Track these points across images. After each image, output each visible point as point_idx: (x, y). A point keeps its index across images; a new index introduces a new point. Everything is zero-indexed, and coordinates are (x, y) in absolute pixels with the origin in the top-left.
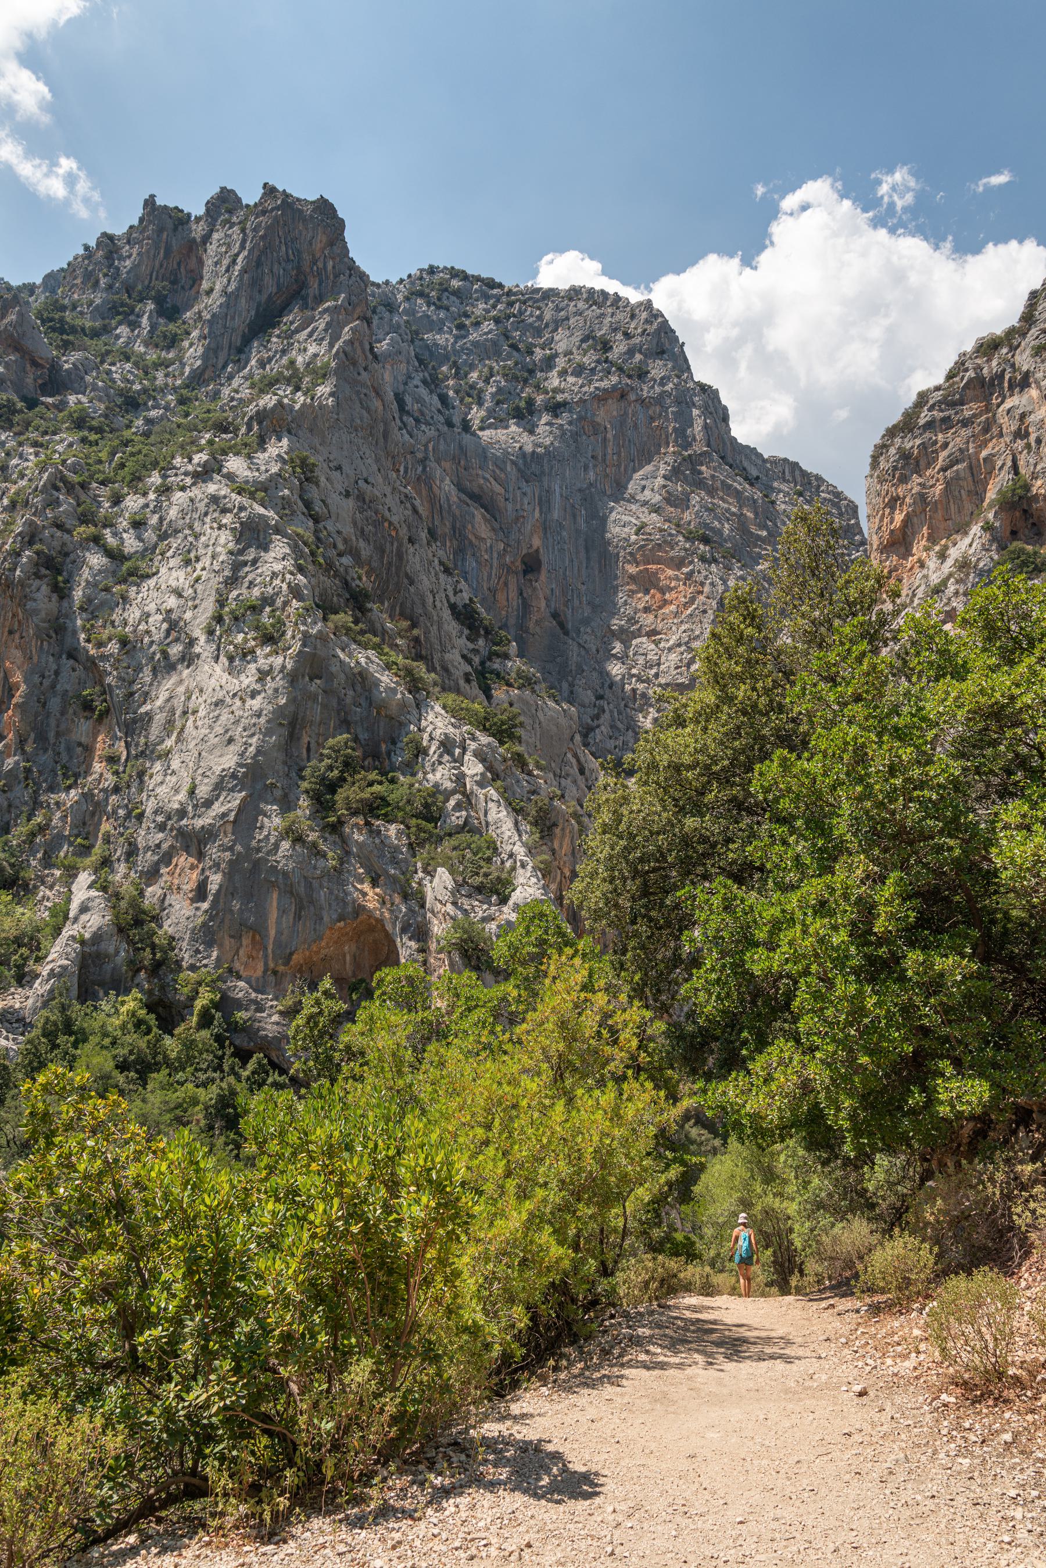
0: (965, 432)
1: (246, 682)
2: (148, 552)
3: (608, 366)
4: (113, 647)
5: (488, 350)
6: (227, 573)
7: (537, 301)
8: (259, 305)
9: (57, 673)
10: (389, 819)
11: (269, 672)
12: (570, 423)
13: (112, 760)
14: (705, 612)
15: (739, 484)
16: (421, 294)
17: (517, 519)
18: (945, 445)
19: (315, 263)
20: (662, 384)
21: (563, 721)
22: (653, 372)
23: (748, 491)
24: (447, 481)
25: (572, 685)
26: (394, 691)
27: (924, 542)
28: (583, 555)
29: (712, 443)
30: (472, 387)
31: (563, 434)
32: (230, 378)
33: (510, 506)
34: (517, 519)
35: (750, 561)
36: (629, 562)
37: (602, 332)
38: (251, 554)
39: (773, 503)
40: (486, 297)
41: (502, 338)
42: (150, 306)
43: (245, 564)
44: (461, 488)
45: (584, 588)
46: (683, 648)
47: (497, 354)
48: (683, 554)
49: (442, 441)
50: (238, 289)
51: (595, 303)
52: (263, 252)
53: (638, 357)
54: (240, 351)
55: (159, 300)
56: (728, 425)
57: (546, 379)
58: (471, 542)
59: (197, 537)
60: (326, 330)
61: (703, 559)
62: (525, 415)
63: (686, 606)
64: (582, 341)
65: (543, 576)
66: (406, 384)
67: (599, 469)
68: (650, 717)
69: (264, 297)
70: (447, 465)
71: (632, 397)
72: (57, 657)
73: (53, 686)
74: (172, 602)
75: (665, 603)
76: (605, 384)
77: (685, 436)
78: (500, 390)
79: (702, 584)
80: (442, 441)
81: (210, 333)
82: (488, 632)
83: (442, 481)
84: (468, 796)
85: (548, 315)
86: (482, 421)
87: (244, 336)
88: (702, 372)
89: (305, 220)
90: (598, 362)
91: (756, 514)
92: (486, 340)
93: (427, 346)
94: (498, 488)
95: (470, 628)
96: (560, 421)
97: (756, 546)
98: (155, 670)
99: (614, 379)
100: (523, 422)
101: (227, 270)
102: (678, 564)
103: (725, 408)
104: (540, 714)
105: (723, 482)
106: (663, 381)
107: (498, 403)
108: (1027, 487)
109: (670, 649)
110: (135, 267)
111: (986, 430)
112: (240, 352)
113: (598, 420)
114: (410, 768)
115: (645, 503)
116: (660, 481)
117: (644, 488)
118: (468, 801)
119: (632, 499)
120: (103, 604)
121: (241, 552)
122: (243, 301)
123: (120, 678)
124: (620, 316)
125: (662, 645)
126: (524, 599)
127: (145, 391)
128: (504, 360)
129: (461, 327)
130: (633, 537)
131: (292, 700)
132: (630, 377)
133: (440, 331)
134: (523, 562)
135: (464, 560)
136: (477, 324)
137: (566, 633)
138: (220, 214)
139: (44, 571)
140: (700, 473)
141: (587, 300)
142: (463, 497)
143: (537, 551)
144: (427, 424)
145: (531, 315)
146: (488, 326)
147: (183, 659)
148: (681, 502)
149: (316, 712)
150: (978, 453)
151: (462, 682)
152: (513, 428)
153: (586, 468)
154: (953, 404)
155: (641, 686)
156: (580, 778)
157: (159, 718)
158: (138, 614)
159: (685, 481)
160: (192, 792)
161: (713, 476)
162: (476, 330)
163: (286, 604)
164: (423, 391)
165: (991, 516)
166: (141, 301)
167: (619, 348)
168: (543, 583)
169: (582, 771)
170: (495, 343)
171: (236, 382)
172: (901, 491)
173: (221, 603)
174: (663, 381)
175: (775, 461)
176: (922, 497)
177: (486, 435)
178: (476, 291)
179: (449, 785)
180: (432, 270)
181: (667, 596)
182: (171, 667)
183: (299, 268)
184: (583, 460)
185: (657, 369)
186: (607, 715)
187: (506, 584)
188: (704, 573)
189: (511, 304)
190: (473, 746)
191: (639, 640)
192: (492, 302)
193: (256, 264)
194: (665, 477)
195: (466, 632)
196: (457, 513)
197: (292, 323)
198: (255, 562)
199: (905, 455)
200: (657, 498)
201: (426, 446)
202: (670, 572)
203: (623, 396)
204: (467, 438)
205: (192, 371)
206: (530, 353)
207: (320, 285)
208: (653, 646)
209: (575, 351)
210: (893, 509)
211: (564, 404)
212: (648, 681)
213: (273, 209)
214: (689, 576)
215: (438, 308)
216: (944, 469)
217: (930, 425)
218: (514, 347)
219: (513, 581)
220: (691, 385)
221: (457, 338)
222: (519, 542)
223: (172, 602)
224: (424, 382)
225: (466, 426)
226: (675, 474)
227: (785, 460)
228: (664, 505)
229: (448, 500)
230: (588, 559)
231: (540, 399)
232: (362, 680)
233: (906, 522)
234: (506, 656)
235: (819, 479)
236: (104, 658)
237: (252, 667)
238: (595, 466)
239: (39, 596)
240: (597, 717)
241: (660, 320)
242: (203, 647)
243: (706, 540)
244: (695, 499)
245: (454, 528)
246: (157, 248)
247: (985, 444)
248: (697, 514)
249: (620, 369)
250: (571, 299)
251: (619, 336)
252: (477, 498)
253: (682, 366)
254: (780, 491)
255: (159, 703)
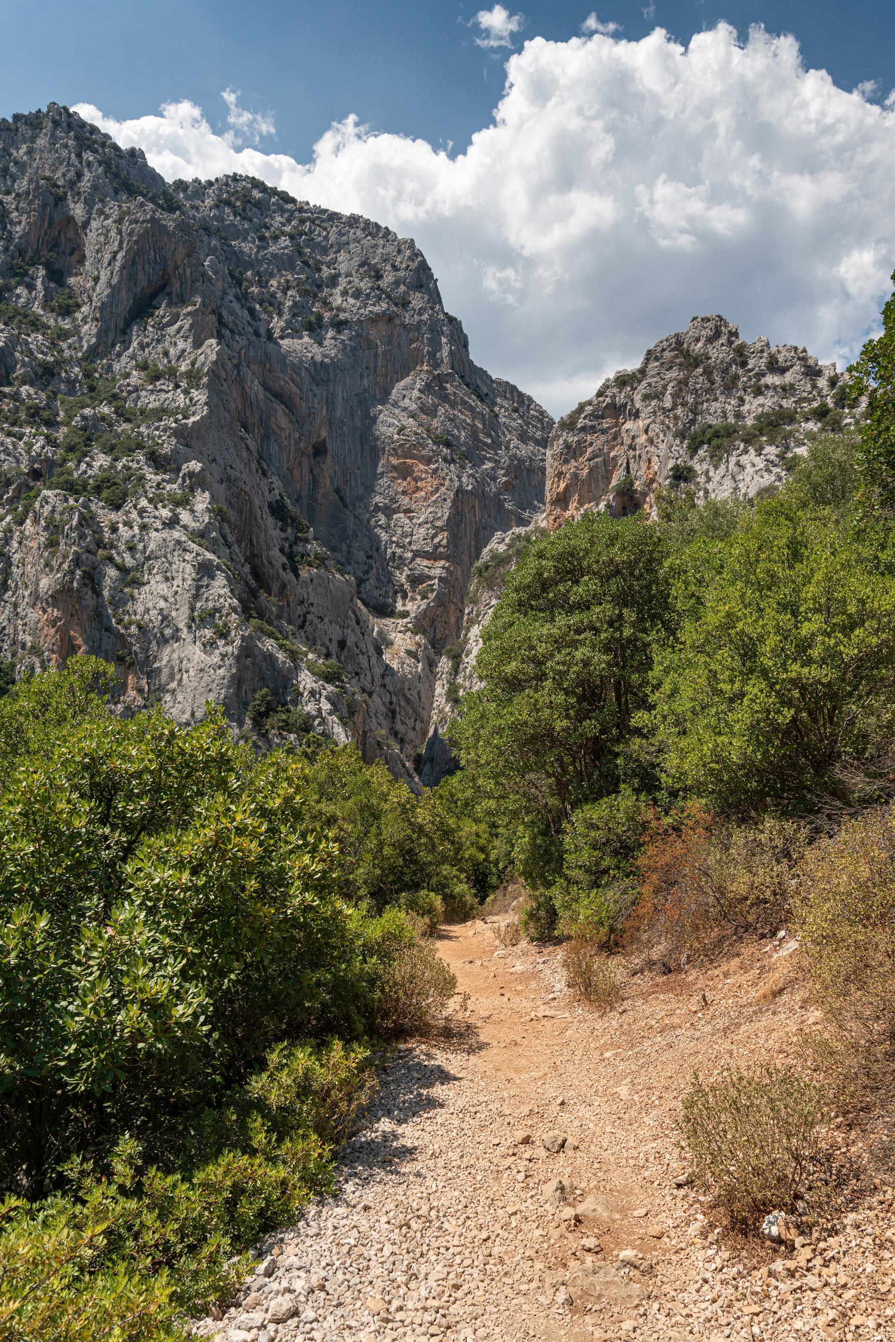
0: (603, 438)
1: (215, 660)
2: (139, 567)
3: (380, 293)
4: (133, 629)
5: (284, 263)
6: (193, 592)
7: (324, 221)
8: (135, 296)
9: (101, 639)
10: (290, 732)
11: (226, 655)
12: (350, 339)
13: (140, 691)
14: (445, 500)
15: (473, 401)
16: (228, 203)
17: (309, 414)
18: (591, 444)
19: (177, 268)
20: (420, 314)
21: (346, 588)
22: (414, 302)
23: (480, 407)
24: (256, 382)
25: (349, 546)
26: (284, 662)
27: (575, 504)
28: (358, 446)
29: (456, 365)
30: (273, 296)
31: (345, 348)
32: (119, 355)
33: (304, 404)
34: (309, 414)
35: (478, 462)
36: (392, 455)
37: (376, 261)
38: (205, 581)
39: (497, 416)
40: (282, 211)
41: (296, 254)
42: (42, 272)
43: (202, 586)
44: (266, 388)
45: (359, 472)
46: (429, 525)
47: (292, 267)
48: (431, 454)
49: (251, 349)
50: (119, 282)
51: (370, 234)
52: (137, 254)
53: (402, 288)
54: (124, 332)
55: (48, 266)
56: (467, 350)
57: (331, 295)
58: (274, 431)
59: (171, 564)
60: (190, 330)
61: (445, 460)
62: (315, 328)
63: (432, 493)
64: (360, 266)
65: (329, 459)
66: (222, 299)
67: (372, 377)
68: (405, 574)
69: (139, 290)
70: (255, 367)
71: (397, 322)
72: (99, 630)
73: (99, 647)
74: (162, 604)
75: (418, 489)
76: (376, 309)
77: (435, 359)
78: (295, 303)
79: (444, 479)
80: (251, 349)
81: (101, 317)
82: (293, 521)
83: (252, 382)
84: (323, 719)
85: (332, 238)
86: (282, 331)
87: (125, 320)
88: (450, 306)
89: (168, 234)
90: (372, 288)
91: (484, 425)
92: (283, 254)
93: (234, 252)
94: (295, 389)
95: (281, 520)
96: (342, 337)
97: (483, 450)
98: (158, 643)
99: (384, 305)
100: (314, 335)
101: (109, 264)
102: (428, 461)
103: (466, 337)
104: (331, 585)
105: (462, 399)
106: (421, 311)
107: (294, 315)
108: (632, 484)
109: (420, 525)
110: (26, 235)
111: (615, 438)
112: (124, 333)
113: (372, 338)
114: (295, 702)
115: (405, 409)
116: (416, 393)
117: (404, 396)
118: (323, 722)
119: (395, 404)
120: (120, 599)
121: (199, 580)
122: (124, 292)
123: (141, 648)
124: (389, 249)
125: (414, 521)
126: (314, 476)
127: (57, 362)
128: (298, 274)
129: (262, 238)
130: (396, 436)
131: (238, 670)
132: (396, 305)
133: (245, 239)
134: (314, 447)
135: (269, 444)
136: (276, 238)
137: (345, 506)
138: (94, 203)
139: (87, 581)
140: (446, 389)
141: (363, 230)
142: (268, 395)
143: (324, 440)
144: (240, 334)
145: (319, 235)
146: (284, 241)
147: (173, 638)
148: (431, 412)
149: (249, 675)
150: (609, 453)
151: (281, 570)
152: (306, 339)
153: (362, 376)
154: (597, 417)
155: (399, 551)
156: (357, 628)
157: (166, 672)
158: (142, 608)
159: (434, 394)
160: (193, 715)
161: (455, 393)
162: (275, 243)
163: (228, 614)
164: (236, 306)
165: (611, 497)
166: (33, 265)
167: (388, 278)
168: (329, 466)
169: (358, 623)
170: (290, 258)
171: (124, 359)
172: (564, 469)
173: (192, 609)
174: (421, 311)
175: (500, 383)
176: (575, 476)
177: (285, 343)
178: (274, 204)
179: (314, 713)
180: (235, 178)
181: (419, 484)
182: (166, 641)
183: (164, 270)
184: (360, 370)
185: (417, 301)
186: (374, 571)
187: (300, 463)
188: (446, 471)
189: (302, 221)
190: (324, 693)
191: (398, 515)
192: (286, 215)
193: (131, 263)
194: (419, 390)
195: (280, 524)
196: (264, 408)
197: (163, 317)
198: (207, 586)
199: (567, 446)
200: (414, 407)
201: (239, 353)
202: (422, 467)
203: (390, 319)
204: (271, 346)
205: (89, 347)
206: (319, 270)
207: (181, 285)
208: (408, 521)
209: (353, 272)
210: (559, 479)
211: (345, 323)
212: (403, 547)
213: (143, 222)
214: (435, 471)
215: (243, 218)
216: (589, 460)
217: (583, 429)
218: (306, 263)
219: (305, 462)
220: (441, 316)
221: (260, 248)
222: (310, 432)
223: (162, 604)
224: (236, 297)
225: (269, 333)
226: (427, 389)
227: (507, 383)
228: (418, 412)
229: (257, 397)
230: (362, 450)
231: (327, 315)
232: (270, 658)
233: (566, 489)
234: (306, 541)
235: (530, 399)
236: (130, 636)
237: (217, 651)
238: (368, 375)
239: (87, 597)
240: (367, 572)
241: (420, 259)
242: (184, 634)
243: (448, 444)
244: (441, 411)
245: (261, 419)
246: (43, 220)
247: (612, 448)
248: (442, 422)
249: (389, 297)
250: (351, 226)
251: (388, 267)
252: (279, 396)
253: (435, 298)
254: (502, 407)
255: (164, 662)
